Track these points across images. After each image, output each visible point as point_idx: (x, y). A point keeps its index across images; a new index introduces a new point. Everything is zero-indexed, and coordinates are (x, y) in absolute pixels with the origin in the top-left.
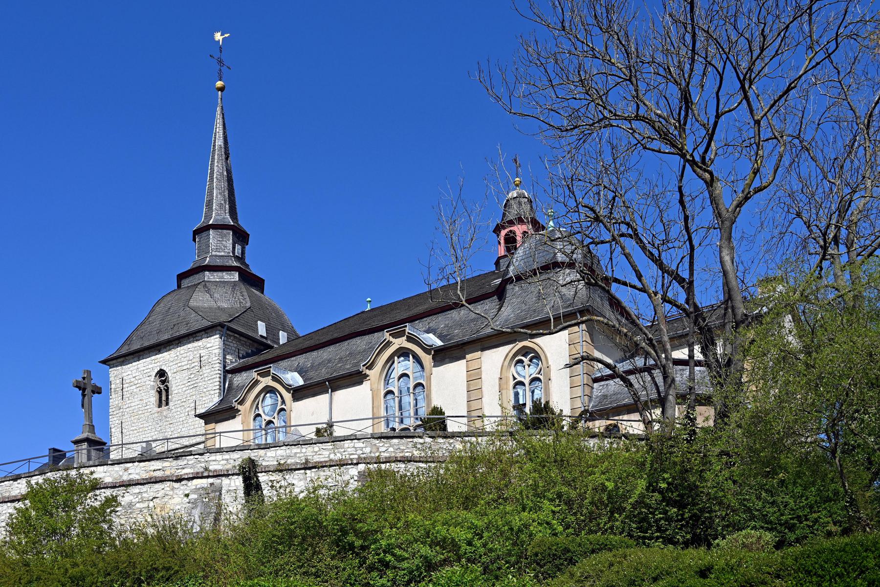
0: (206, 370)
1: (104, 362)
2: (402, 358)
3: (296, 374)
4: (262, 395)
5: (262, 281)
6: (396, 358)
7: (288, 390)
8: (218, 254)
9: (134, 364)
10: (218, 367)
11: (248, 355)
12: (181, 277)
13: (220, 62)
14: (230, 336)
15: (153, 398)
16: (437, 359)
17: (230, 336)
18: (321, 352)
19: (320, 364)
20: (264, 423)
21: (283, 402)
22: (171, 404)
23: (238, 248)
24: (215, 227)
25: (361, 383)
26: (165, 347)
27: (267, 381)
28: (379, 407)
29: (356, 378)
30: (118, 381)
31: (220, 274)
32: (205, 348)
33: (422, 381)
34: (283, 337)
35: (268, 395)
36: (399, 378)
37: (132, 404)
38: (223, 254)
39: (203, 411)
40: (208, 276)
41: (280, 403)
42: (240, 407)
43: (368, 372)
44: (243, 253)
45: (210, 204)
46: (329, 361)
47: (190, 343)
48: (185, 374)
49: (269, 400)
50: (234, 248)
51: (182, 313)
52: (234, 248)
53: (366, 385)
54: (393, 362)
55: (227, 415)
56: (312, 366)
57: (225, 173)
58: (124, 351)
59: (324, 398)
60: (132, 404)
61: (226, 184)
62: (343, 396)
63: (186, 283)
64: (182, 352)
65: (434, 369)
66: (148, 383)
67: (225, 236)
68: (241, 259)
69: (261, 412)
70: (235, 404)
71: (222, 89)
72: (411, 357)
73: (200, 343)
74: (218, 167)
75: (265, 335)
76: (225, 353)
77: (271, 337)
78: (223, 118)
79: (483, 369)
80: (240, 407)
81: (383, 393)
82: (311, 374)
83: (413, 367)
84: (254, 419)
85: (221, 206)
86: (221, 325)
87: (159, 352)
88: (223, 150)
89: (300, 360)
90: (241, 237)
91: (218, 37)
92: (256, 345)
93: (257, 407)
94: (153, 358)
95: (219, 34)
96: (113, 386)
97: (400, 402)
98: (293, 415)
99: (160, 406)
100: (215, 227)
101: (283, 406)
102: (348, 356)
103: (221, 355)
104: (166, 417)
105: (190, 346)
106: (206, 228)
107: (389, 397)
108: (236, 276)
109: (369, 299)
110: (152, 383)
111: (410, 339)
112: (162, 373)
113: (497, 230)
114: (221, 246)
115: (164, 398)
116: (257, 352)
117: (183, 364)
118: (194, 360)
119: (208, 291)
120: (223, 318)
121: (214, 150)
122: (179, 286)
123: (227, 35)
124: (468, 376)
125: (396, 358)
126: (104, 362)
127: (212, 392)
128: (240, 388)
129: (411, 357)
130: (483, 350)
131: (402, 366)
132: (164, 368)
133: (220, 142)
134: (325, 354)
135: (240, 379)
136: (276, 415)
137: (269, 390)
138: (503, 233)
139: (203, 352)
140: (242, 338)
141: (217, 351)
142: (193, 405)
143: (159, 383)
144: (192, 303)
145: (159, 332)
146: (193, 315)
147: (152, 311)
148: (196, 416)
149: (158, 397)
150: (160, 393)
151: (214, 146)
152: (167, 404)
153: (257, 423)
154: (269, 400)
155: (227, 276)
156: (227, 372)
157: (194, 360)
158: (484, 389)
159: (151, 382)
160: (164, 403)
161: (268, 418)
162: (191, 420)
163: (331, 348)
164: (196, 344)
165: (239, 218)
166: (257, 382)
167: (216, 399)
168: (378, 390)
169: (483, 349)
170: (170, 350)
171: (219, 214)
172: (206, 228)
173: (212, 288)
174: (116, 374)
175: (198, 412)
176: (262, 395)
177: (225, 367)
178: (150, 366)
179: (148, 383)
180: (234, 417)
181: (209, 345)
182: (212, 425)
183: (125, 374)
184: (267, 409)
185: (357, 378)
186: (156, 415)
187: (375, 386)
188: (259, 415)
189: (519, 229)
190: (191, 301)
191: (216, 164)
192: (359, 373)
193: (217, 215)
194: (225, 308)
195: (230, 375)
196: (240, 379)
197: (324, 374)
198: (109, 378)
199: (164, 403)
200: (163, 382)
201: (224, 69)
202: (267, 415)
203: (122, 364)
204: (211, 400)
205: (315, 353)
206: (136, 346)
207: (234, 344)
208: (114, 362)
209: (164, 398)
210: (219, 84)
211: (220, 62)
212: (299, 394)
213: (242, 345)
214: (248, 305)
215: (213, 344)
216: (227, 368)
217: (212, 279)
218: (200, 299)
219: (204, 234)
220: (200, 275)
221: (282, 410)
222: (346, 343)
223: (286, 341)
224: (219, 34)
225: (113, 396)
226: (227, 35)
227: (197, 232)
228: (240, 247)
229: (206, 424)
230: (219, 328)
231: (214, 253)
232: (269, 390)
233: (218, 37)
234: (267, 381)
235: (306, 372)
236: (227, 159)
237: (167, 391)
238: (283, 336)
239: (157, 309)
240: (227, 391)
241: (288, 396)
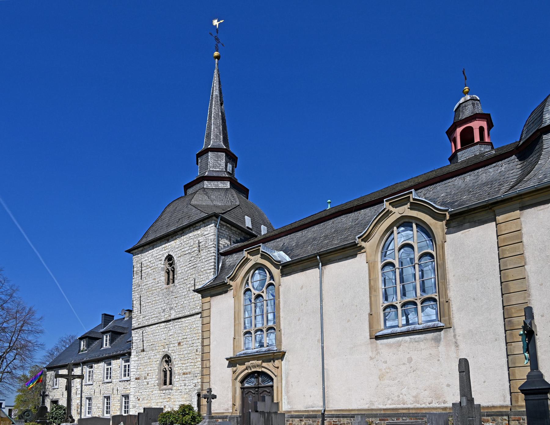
0: (203, 253)
1: (129, 251)
2: (402, 229)
3: (282, 253)
4: (252, 272)
5: (248, 190)
6: (395, 228)
7: (276, 266)
8: (214, 170)
9: (150, 251)
10: (213, 250)
11: (237, 242)
12: (187, 187)
13: (217, 39)
14: (224, 225)
15: (163, 277)
16: (453, 224)
17: (224, 225)
18: (305, 232)
19: (304, 243)
20: (253, 297)
21: (272, 277)
22: (176, 281)
23: (230, 166)
24: (213, 150)
25: (354, 256)
26: (172, 237)
27: (257, 259)
28: (376, 280)
29: (350, 251)
30: (138, 265)
31: (216, 183)
32: (203, 235)
33: (431, 251)
34: (264, 230)
35: (257, 272)
36: (400, 249)
37: (148, 283)
38: (218, 170)
39: (200, 287)
40: (207, 184)
41: (268, 278)
42: (231, 283)
43: (363, 244)
44: (233, 170)
45: (209, 135)
46: (314, 239)
47: (191, 232)
48: (188, 257)
49: (258, 277)
50: (226, 166)
51: (186, 210)
52: (226, 166)
53: (361, 258)
54: (393, 232)
55: (220, 290)
56: (297, 245)
57: (220, 114)
58: (143, 242)
59: (314, 273)
60: (148, 283)
61: (221, 121)
62: (332, 269)
63: (190, 191)
64: (185, 240)
65: (448, 237)
66: (159, 265)
67: (220, 157)
68: (232, 174)
69: (250, 287)
70: (227, 281)
71: (218, 57)
72: (414, 226)
73: (199, 232)
74: (215, 109)
75: (251, 227)
76: (219, 236)
77: (255, 229)
78: (219, 77)
79: (524, 231)
80: (231, 283)
81: (380, 265)
82: (297, 252)
83: (418, 237)
84: (245, 293)
85: (217, 136)
86: (216, 215)
87: (168, 241)
88: (219, 98)
89: (280, 242)
90: (231, 158)
91: (216, 23)
92: (243, 234)
93: (247, 283)
94: (163, 246)
95: (216, 20)
96: (135, 269)
97: (401, 274)
98: (281, 289)
99: (168, 284)
100: (213, 150)
101: (272, 281)
102: (334, 233)
103: (216, 240)
104: (172, 292)
105: (191, 235)
106: (207, 151)
107: (388, 269)
108: (228, 185)
109: (329, 201)
110: (162, 266)
111: (415, 206)
112: (170, 258)
113: (450, 132)
114: (216, 163)
115: (171, 277)
116: (246, 239)
117: (185, 249)
118: (194, 246)
119: (206, 194)
120: (218, 211)
121: (212, 98)
122: (186, 194)
123: (221, 21)
124: (521, 236)
125: (395, 228)
126: (129, 251)
127: (208, 271)
128: (231, 267)
129: (414, 226)
130: (522, 208)
131: (401, 237)
132: (171, 253)
133: (216, 93)
134: (309, 234)
135: (231, 260)
136: (264, 289)
137: (258, 267)
138: (459, 130)
139: (201, 239)
140: (232, 228)
141: (212, 237)
142: (193, 282)
143: (167, 265)
144: (193, 202)
145: (168, 226)
146: (194, 209)
147: (164, 212)
148: (194, 291)
149: (167, 276)
150: (168, 273)
151: (212, 96)
152: (173, 282)
153: (247, 297)
154: (258, 277)
155: (221, 185)
156: (222, 254)
157: (194, 246)
158: (527, 254)
159: (162, 264)
160: (171, 281)
161: (257, 292)
162: (191, 295)
163: (316, 228)
164: (196, 233)
165: (229, 144)
166: (247, 260)
167: (212, 277)
168: (375, 262)
169: (523, 208)
170: (176, 239)
171: (215, 139)
172: (207, 151)
173: (210, 192)
174: (137, 259)
175: (197, 287)
176: (252, 272)
177: (218, 250)
178: (161, 253)
179: (159, 265)
180: (226, 292)
181: (206, 233)
182: (208, 299)
183: (143, 260)
184: (256, 284)
185: (351, 252)
186: (165, 290)
187: (371, 259)
188: (249, 290)
189: (476, 125)
190: (193, 200)
191: (213, 108)
192: (225, 284)
193: (214, 142)
194: (219, 206)
195: (223, 257)
196: (231, 260)
197: (310, 250)
198: (132, 263)
199: (171, 281)
200: (171, 265)
201: (219, 45)
202: (256, 289)
203: (142, 252)
204: (207, 277)
205: (299, 234)
206: (151, 238)
207: (226, 232)
208: (136, 251)
209: (171, 277)
210: (216, 54)
211: (217, 39)
212: (287, 269)
213: (233, 233)
214: (238, 203)
215: (210, 230)
216: (221, 251)
217: (210, 186)
218: (199, 199)
219: (204, 156)
220: (201, 183)
221: (271, 284)
222: (331, 222)
223: (266, 232)
224: (216, 20)
225: (135, 276)
226: (221, 21)
227: (199, 155)
228: (231, 166)
229: (203, 297)
230: (214, 218)
231: (211, 169)
232: (258, 267)
233: (216, 23)
234: (257, 259)
235: (291, 250)
236: (221, 104)
237: (173, 271)
238: (264, 229)
239: (168, 210)
240: (221, 271)
241: (276, 272)
